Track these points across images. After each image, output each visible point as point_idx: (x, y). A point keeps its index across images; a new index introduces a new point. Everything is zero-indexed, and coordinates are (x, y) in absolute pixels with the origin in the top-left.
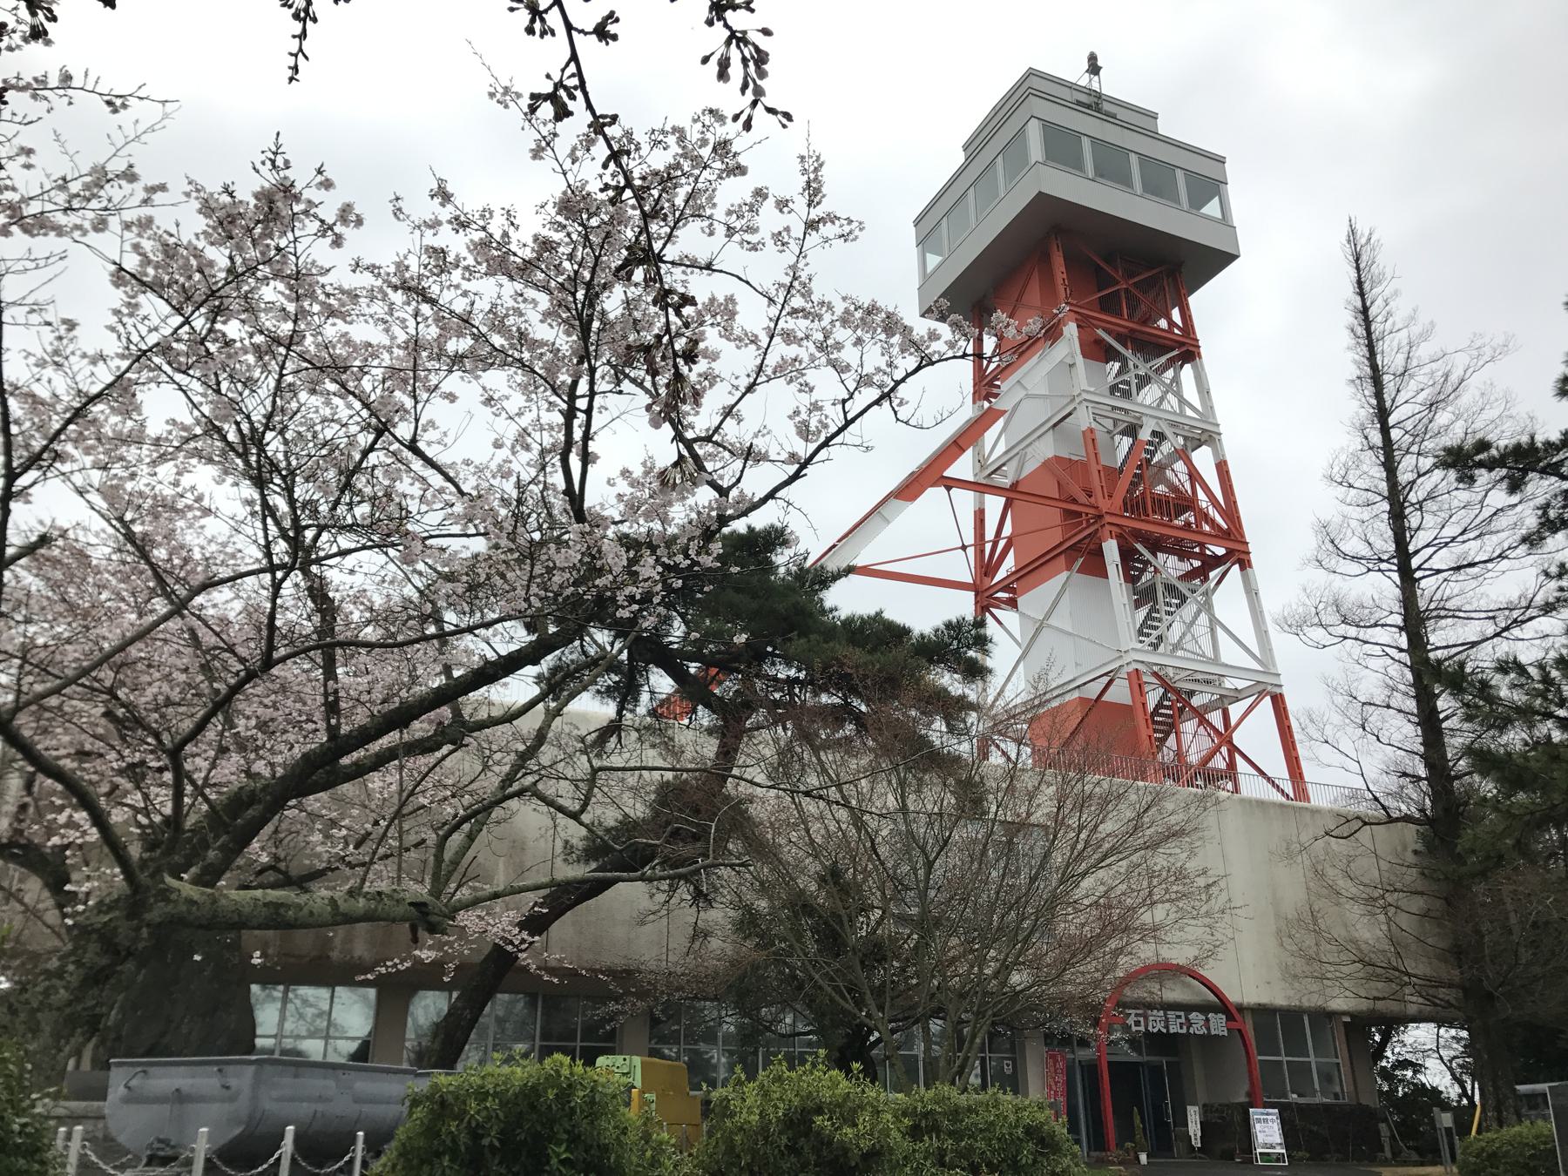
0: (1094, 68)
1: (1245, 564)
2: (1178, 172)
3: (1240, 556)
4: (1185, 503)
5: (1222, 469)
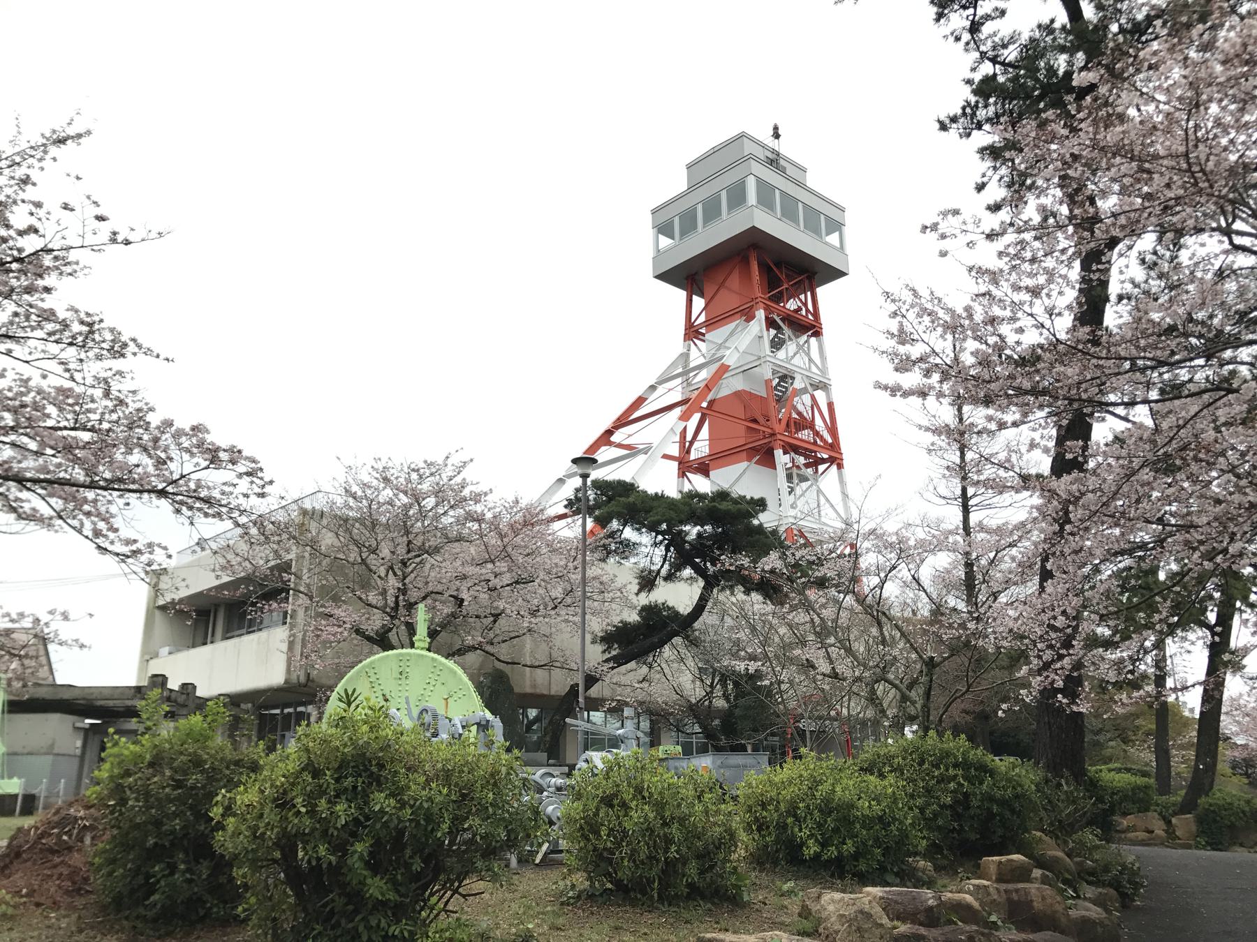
0: (777, 135)
1: (840, 466)
2: (777, 191)
3: (836, 460)
5: (830, 406)
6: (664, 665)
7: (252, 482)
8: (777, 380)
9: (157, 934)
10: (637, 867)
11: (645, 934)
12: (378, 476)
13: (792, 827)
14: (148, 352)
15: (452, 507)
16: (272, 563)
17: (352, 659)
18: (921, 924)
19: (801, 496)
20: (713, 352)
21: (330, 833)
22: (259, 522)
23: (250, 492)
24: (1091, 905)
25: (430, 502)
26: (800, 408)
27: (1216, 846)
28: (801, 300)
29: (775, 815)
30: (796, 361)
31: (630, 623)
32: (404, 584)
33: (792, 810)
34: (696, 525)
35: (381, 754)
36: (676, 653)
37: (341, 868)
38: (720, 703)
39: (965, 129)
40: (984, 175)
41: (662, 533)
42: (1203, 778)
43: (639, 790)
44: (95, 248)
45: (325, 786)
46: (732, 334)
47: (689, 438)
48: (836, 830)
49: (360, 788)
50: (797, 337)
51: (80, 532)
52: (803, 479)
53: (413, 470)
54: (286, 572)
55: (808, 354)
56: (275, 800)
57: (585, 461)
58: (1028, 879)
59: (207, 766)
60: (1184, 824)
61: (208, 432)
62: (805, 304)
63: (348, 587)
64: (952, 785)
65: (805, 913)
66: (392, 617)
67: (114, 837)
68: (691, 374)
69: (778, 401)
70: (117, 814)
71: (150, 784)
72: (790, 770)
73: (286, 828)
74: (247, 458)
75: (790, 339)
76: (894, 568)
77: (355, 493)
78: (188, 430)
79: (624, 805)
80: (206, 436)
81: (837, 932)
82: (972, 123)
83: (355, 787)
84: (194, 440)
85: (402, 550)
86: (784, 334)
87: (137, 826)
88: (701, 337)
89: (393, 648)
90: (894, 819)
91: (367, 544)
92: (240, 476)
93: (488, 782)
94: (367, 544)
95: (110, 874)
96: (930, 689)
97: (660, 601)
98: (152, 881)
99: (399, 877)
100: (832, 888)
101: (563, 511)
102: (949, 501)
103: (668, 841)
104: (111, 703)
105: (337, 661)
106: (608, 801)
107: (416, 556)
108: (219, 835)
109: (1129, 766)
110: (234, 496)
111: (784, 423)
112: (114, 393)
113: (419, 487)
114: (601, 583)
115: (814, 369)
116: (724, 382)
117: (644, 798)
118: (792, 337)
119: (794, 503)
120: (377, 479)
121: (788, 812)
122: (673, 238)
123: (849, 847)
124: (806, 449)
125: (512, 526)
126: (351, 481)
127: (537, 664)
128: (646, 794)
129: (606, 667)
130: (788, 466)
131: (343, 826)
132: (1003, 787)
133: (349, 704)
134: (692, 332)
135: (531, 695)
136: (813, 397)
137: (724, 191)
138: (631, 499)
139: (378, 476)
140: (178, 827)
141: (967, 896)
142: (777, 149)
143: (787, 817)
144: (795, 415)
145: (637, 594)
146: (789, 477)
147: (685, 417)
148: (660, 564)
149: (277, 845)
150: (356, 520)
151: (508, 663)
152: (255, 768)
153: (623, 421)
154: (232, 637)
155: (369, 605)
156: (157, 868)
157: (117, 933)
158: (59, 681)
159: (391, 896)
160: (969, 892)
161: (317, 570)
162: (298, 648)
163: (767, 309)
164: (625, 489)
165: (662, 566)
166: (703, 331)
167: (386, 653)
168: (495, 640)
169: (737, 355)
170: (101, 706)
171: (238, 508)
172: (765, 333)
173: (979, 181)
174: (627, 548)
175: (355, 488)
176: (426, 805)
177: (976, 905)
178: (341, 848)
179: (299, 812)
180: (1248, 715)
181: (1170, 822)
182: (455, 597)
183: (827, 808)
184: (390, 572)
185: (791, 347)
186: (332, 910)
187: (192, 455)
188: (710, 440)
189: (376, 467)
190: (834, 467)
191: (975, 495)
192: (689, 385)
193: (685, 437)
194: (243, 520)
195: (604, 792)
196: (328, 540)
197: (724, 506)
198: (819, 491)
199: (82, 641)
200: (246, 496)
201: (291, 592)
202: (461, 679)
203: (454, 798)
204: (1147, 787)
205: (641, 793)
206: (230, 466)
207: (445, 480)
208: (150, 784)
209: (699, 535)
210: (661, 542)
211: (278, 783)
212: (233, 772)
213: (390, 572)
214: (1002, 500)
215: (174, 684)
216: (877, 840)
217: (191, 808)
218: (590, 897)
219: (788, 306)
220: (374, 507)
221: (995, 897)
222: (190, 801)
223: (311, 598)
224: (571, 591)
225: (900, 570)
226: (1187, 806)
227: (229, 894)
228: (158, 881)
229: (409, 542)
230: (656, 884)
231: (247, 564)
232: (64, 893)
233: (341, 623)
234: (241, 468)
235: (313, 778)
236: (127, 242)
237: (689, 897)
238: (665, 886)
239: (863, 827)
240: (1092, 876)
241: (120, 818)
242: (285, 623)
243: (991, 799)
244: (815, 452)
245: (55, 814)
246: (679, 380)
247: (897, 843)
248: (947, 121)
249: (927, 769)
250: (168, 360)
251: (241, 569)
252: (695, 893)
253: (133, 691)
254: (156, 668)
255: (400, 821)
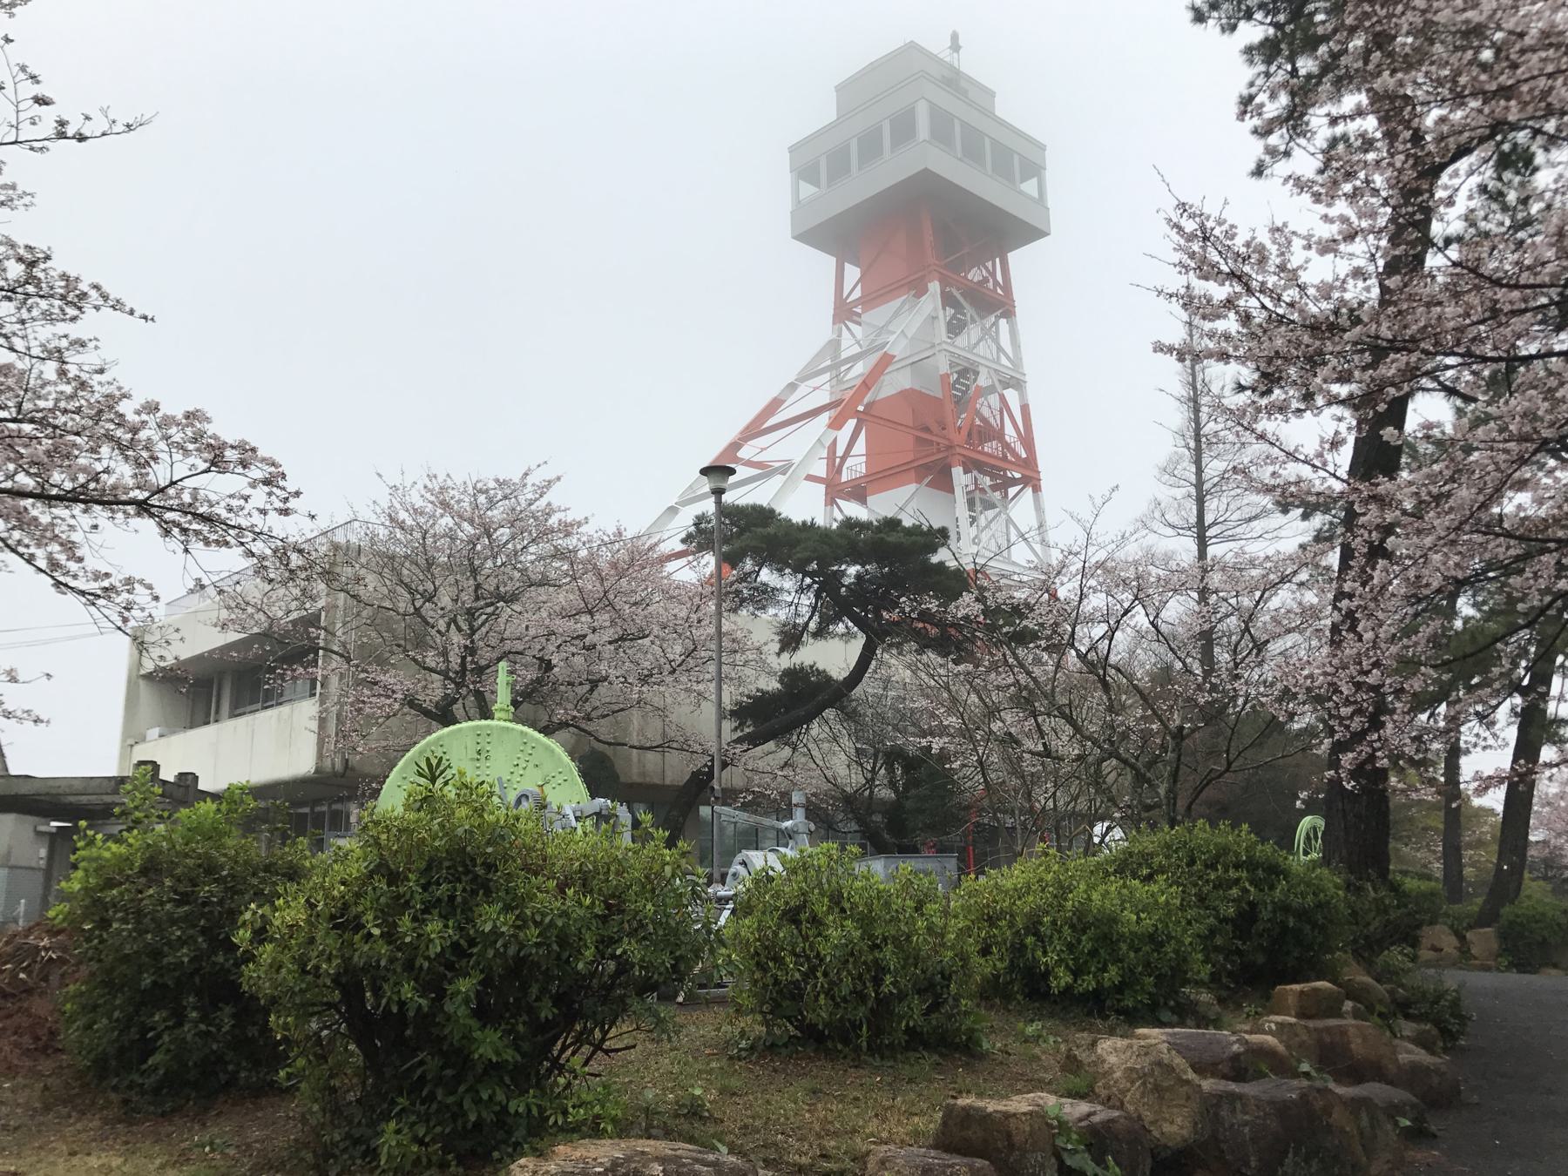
0: (955, 46)
1: (1037, 489)
3: (1031, 480)
4: (993, 433)
5: (1025, 409)
6: (811, 746)
7: (270, 494)
8: (955, 376)
9: (160, 1111)
10: (837, 1005)
11: (856, 1099)
12: (433, 498)
13: (1033, 951)
14: (117, 306)
15: (533, 540)
16: (294, 615)
17: (404, 741)
18: (1225, 1077)
19: (986, 527)
20: (872, 337)
21: (417, 964)
22: (281, 554)
23: (268, 506)
24: (1411, 1046)
25: (503, 534)
26: (986, 412)
27: (1523, 966)
28: (986, 268)
29: (1008, 933)
30: (982, 349)
31: (768, 692)
32: (472, 642)
33: (1033, 926)
34: (855, 563)
35: (490, 850)
36: (827, 729)
37: (434, 1016)
38: (885, 793)
39: (1229, 18)
40: (1252, 84)
41: (811, 575)
42: (1505, 885)
43: (836, 899)
44: (36, 145)
45: (408, 896)
46: (896, 314)
47: (840, 452)
48: (1093, 953)
49: (459, 899)
50: (982, 318)
51: (29, 561)
52: (989, 505)
53: (480, 491)
54: (314, 626)
55: (996, 340)
56: (333, 917)
57: (718, 471)
58: (1338, 1014)
59: (225, 873)
60: (1483, 940)
61: (208, 420)
62: (993, 274)
63: (399, 646)
64: (1235, 892)
65: (1071, 1064)
66: (457, 684)
67: (93, 974)
68: (843, 368)
69: (957, 403)
70: (96, 941)
71: (142, 900)
72: (1014, 876)
73: (350, 958)
74: (263, 460)
75: (973, 321)
76: (1127, 612)
77: (403, 522)
78: (180, 416)
79: (815, 920)
80: (207, 426)
81: (1124, 1092)
82: (1240, 10)
83: (452, 898)
84: (189, 431)
85: (467, 598)
86: (964, 315)
87: (126, 959)
88: (855, 318)
89: (455, 721)
90: (1170, 937)
91: (421, 588)
92: (253, 485)
93: (644, 887)
94: (421, 588)
95: (89, 1027)
96: (1178, 768)
97: (808, 662)
98: (150, 1035)
99: (521, 1028)
100: (1112, 1032)
101: (681, 547)
102: (1181, 532)
103: (880, 970)
104: (84, 799)
105: (384, 743)
106: (792, 916)
107: (488, 605)
108: (249, 970)
109: (1404, 868)
110: (246, 512)
111: (964, 432)
112: (73, 371)
113: (489, 513)
114: (734, 641)
115: (1004, 361)
116: (886, 379)
117: (843, 910)
118: (976, 317)
119: (976, 537)
120: (432, 503)
121: (1026, 928)
122: (819, 187)
123: (1112, 974)
124: (993, 467)
125: (614, 565)
126: (398, 506)
127: (648, 745)
128: (847, 905)
129: (739, 748)
130: (969, 489)
131: (438, 955)
132: (1302, 893)
133: (433, 780)
134: (844, 312)
135: (640, 784)
136: (1003, 399)
137: (887, 121)
138: (771, 530)
139: (433, 498)
140: (186, 960)
141: (1269, 1038)
142: (956, 65)
143: (1026, 935)
144: (978, 422)
145: (778, 654)
146: (971, 504)
147: (836, 424)
148: (808, 616)
149: (336, 980)
150: (406, 557)
151: (610, 744)
152: (294, 874)
153: (754, 430)
154: (244, 714)
155: (425, 668)
156: (157, 1018)
157: (102, 1109)
158: (13, 771)
159: (510, 1055)
160: (1270, 1032)
161: (354, 624)
162: (332, 727)
163: (944, 282)
164: (763, 516)
165: (811, 618)
166: (858, 310)
167: (446, 730)
168: (594, 714)
169: (904, 342)
170: (71, 804)
171: (251, 528)
172: (941, 313)
173: (1245, 92)
174: (764, 597)
175: (403, 515)
176: (560, 923)
177: (1281, 1048)
178: (435, 987)
179: (370, 935)
180: (1549, 804)
181: (1464, 937)
182: (541, 659)
183: (1081, 922)
184: (452, 626)
185: (974, 332)
186: (422, 1077)
187: (186, 452)
188: (867, 455)
189: (430, 486)
190: (1029, 490)
191: (1214, 524)
192: (840, 382)
193: (835, 452)
194: (258, 547)
195: (787, 903)
196: (372, 585)
197: (892, 538)
198: (1009, 521)
199: (37, 712)
200: (263, 512)
201: (321, 652)
202: (560, 759)
203: (598, 911)
204: (1433, 894)
205: (838, 903)
206: (239, 469)
207: (524, 504)
208: (142, 900)
209: (859, 577)
210: (809, 586)
211: (335, 893)
212: (263, 881)
213: (452, 626)
214: (1248, 529)
215: (168, 774)
216: (1147, 964)
217: (204, 931)
218: (765, 1050)
219: (970, 277)
220: (429, 541)
221: (1305, 1038)
222: (202, 922)
223: (348, 660)
224: (695, 650)
225: (1133, 616)
226: (1487, 917)
227: (269, 1054)
228: (159, 1036)
229: (478, 587)
230: (864, 1028)
231: (261, 616)
232: (23, 1054)
233: (390, 693)
234: (256, 473)
235: (389, 885)
236: (81, 138)
237: (908, 1047)
238: (876, 1032)
239: (1131, 947)
240: (1404, 1008)
241: (101, 947)
242: (314, 695)
243: (1285, 908)
244: (1005, 470)
245: (7, 943)
246: (827, 376)
247: (1172, 968)
248: (1205, 8)
249: (1200, 871)
250: (145, 318)
251: (253, 623)
252: (916, 1040)
253: (113, 783)
254: (142, 753)
255: (522, 946)
